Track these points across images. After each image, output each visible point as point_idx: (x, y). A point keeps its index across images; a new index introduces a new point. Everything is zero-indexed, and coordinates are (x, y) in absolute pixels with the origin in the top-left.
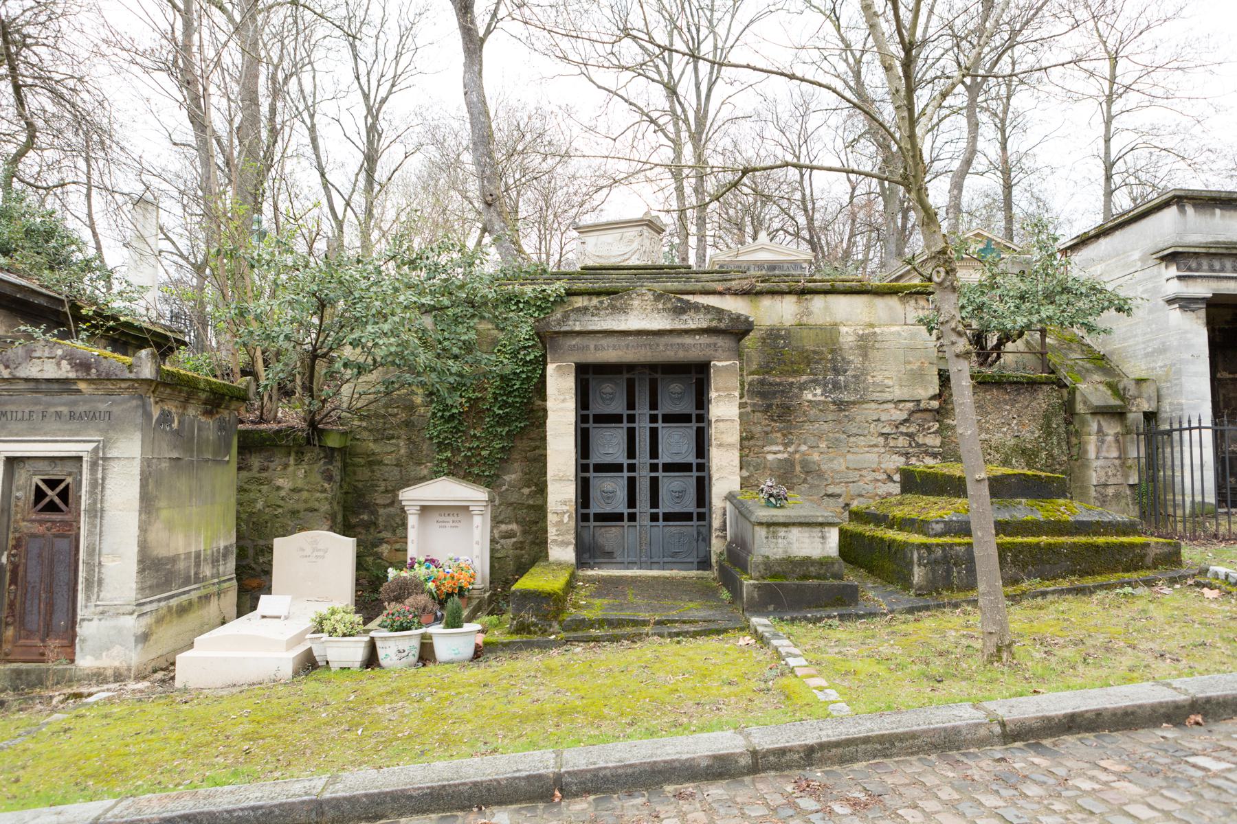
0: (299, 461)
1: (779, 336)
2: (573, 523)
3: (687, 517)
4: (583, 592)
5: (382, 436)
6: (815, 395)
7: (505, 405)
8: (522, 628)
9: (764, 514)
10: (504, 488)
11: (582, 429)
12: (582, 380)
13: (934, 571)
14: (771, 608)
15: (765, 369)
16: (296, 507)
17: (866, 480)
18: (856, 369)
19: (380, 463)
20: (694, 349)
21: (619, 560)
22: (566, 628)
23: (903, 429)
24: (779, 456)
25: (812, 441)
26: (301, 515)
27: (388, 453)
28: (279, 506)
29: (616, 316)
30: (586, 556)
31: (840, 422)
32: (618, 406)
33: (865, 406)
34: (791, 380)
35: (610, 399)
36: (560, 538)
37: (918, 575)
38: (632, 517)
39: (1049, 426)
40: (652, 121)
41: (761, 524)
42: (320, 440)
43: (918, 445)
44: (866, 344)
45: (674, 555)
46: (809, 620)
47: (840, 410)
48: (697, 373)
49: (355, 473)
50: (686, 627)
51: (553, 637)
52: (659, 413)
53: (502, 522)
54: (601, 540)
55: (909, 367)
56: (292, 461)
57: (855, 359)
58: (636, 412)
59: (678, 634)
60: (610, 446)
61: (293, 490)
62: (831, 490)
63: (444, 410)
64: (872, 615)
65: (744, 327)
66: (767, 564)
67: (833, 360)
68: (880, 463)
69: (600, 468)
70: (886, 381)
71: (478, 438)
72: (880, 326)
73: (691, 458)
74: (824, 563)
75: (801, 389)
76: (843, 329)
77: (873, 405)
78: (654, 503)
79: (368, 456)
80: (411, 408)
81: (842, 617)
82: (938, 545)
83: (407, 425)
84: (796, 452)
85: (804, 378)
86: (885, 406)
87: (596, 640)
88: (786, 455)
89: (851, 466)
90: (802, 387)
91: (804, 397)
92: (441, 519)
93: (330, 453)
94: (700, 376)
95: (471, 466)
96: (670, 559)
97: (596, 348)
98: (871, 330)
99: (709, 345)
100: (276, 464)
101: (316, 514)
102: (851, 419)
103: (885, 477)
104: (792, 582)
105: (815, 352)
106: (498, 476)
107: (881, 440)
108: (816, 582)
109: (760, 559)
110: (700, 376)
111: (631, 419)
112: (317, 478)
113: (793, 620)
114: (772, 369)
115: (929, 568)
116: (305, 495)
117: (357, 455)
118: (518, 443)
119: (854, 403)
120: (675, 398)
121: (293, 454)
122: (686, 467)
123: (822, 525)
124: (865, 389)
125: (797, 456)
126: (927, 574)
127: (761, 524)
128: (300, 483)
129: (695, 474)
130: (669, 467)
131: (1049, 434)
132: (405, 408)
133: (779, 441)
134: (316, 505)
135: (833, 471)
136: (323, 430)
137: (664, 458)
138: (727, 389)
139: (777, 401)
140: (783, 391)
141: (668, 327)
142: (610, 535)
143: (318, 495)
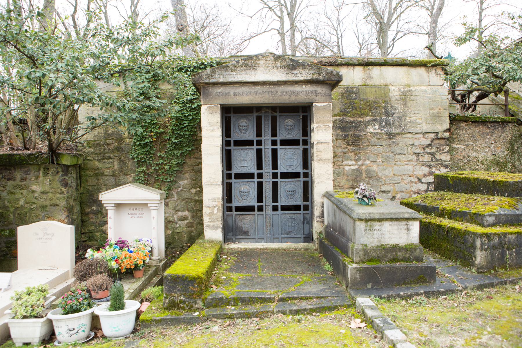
0: (46, 174)
1: (352, 92)
2: (220, 214)
3: (297, 208)
4: (225, 266)
5: (104, 158)
6: (375, 129)
7: (178, 136)
8: (173, 305)
9: (362, 211)
10: (179, 189)
11: (227, 150)
12: (226, 118)
13: (492, 254)
14: (369, 286)
15: (344, 112)
16: (45, 203)
17: (405, 181)
18: (400, 113)
19: (103, 174)
20: (300, 94)
21: (252, 236)
22: (208, 305)
23: (427, 150)
24: (353, 167)
25: (372, 158)
26: (48, 209)
27: (107, 168)
28: (34, 203)
29: (248, 72)
30: (231, 234)
31: (390, 146)
32: (250, 135)
33: (405, 136)
34: (360, 119)
35: (244, 129)
36: (212, 224)
37: (480, 257)
38: (260, 209)
39: (513, 148)
40: (270, 8)
41: (361, 220)
42: (57, 160)
43: (437, 160)
44: (406, 97)
45: (288, 233)
46: (402, 298)
47: (390, 138)
48: (303, 112)
49: (87, 181)
50: (304, 305)
51: (197, 314)
52: (278, 139)
53: (179, 211)
54: (240, 224)
55: (431, 112)
56: (41, 174)
57: (399, 107)
58: (263, 138)
59: (297, 312)
60: (244, 161)
61: (43, 193)
62: (384, 188)
63: (141, 140)
64: (449, 292)
65: (336, 79)
66: (366, 251)
67: (386, 107)
68: (414, 171)
69: (239, 176)
70: (418, 120)
71: (163, 158)
72: (414, 86)
73: (299, 169)
74: (408, 249)
75: (366, 125)
76: (392, 88)
77: (410, 135)
78: (275, 198)
79: (95, 170)
80: (120, 139)
81: (427, 294)
82: (495, 234)
83: (118, 151)
84: (363, 165)
85: (368, 118)
86: (417, 136)
87: (231, 317)
88: (356, 167)
89: (396, 173)
90: (367, 124)
91: (368, 130)
92: (132, 212)
93: (66, 169)
94: (305, 114)
95: (158, 175)
96: (286, 236)
97: (235, 94)
98: (409, 88)
99: (312, 92)
100: (31, 176)
101: (57, 207)
102: (396, 144)
103: (417, 180)
104: (384, 265)
105: (374, 102)
106: (176, 182)
107: (415, 157)
108: (403, 264)
109: (360, 247)
110: (305, 114)
111: (259, 143)
112: (57, 184)
113: (389, 298)
114: (348, 113)
115: (488, 251)
116: (50, 195)
117: (88, 170)
118: (188, 160)
119: (398, 134)
120: (288, 129)
121: (42, 170)
122: (296, 175)
123: (407, 219)
124: (405, 125)
125: (363, 167)
126: (487, 256)
127: (361, 220)
128: (47, 188)
129: (302, 179)
130: (285, 175)
131: (513, 153)
132: (117, 140)
133: (353, 158)
134: (58, 202)
135: (386, 176)
136: (59, 154)
137: (282, 169)
138: (324, 122)
139: (351, 133)
140: (355, 127)
141: (284, 79)
142: (246, 221)
143: (58, 195)
